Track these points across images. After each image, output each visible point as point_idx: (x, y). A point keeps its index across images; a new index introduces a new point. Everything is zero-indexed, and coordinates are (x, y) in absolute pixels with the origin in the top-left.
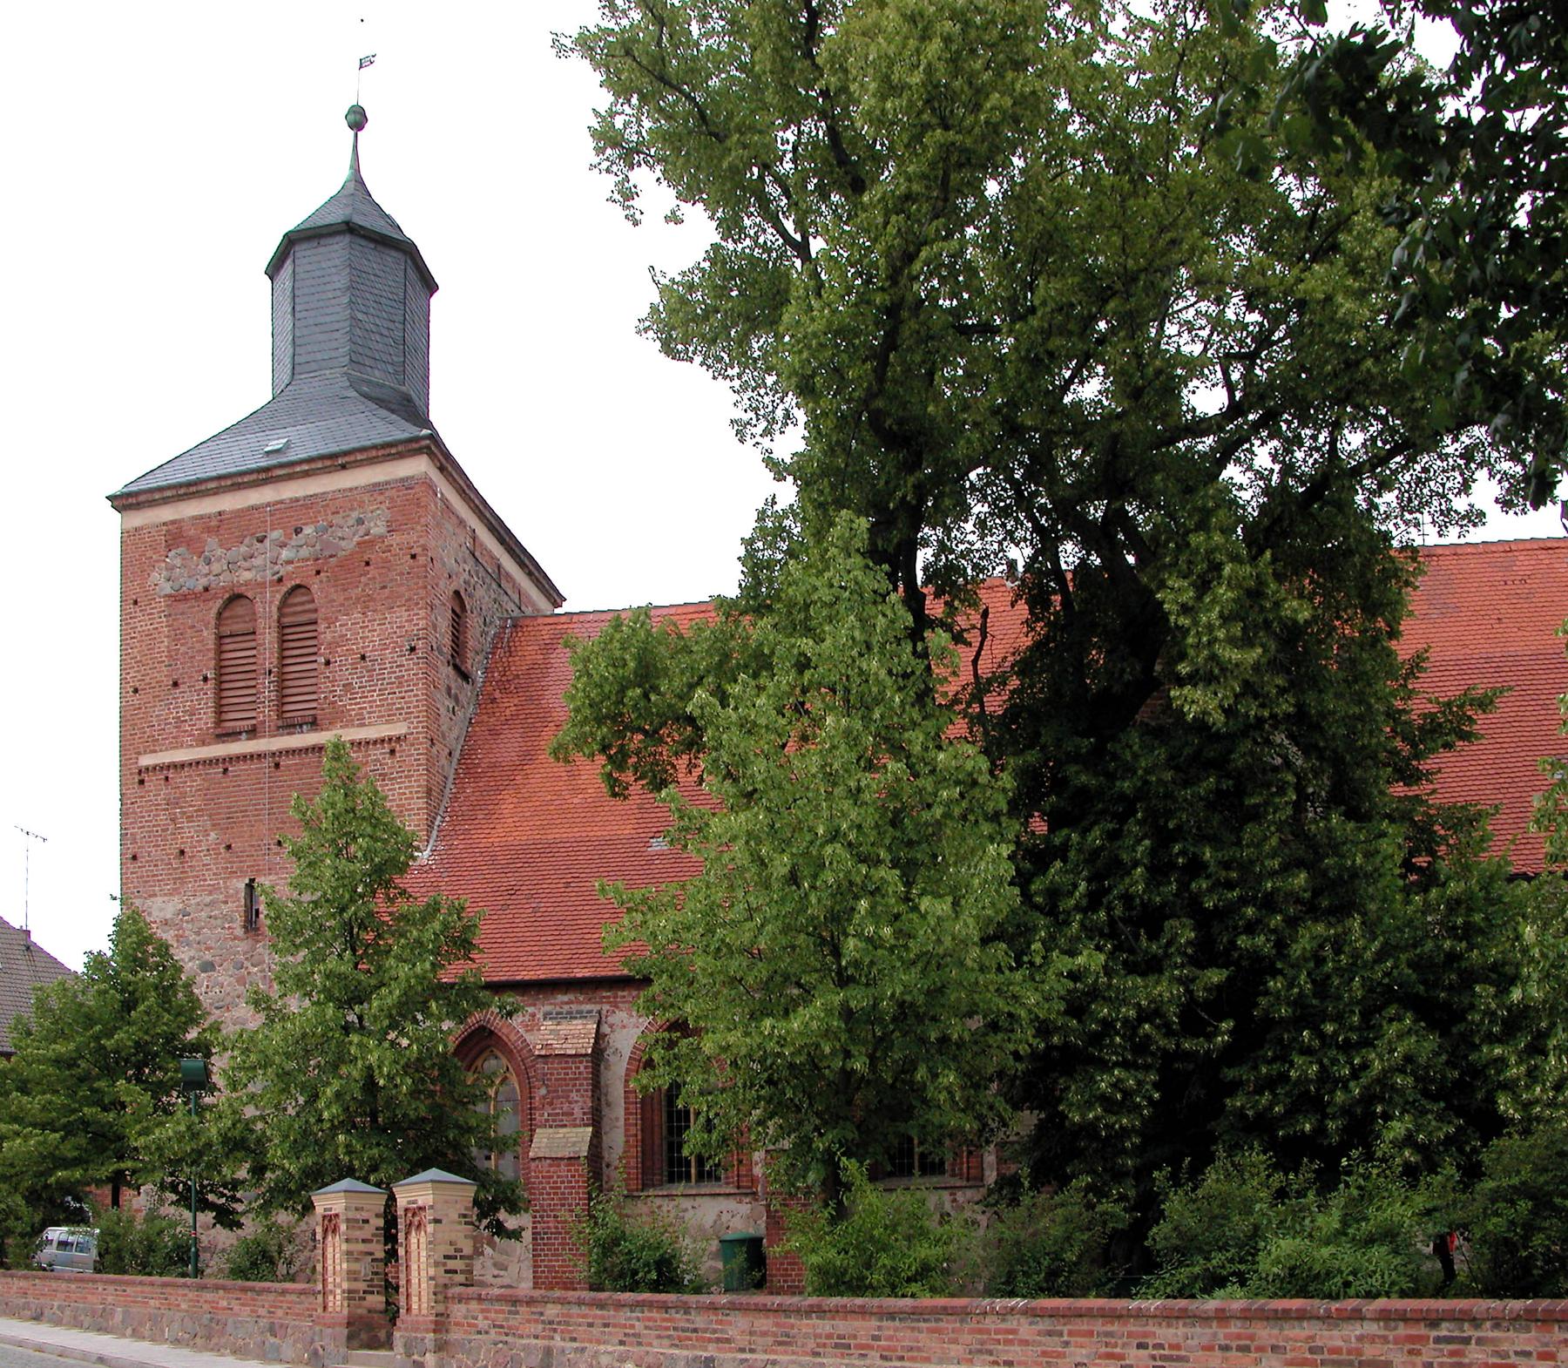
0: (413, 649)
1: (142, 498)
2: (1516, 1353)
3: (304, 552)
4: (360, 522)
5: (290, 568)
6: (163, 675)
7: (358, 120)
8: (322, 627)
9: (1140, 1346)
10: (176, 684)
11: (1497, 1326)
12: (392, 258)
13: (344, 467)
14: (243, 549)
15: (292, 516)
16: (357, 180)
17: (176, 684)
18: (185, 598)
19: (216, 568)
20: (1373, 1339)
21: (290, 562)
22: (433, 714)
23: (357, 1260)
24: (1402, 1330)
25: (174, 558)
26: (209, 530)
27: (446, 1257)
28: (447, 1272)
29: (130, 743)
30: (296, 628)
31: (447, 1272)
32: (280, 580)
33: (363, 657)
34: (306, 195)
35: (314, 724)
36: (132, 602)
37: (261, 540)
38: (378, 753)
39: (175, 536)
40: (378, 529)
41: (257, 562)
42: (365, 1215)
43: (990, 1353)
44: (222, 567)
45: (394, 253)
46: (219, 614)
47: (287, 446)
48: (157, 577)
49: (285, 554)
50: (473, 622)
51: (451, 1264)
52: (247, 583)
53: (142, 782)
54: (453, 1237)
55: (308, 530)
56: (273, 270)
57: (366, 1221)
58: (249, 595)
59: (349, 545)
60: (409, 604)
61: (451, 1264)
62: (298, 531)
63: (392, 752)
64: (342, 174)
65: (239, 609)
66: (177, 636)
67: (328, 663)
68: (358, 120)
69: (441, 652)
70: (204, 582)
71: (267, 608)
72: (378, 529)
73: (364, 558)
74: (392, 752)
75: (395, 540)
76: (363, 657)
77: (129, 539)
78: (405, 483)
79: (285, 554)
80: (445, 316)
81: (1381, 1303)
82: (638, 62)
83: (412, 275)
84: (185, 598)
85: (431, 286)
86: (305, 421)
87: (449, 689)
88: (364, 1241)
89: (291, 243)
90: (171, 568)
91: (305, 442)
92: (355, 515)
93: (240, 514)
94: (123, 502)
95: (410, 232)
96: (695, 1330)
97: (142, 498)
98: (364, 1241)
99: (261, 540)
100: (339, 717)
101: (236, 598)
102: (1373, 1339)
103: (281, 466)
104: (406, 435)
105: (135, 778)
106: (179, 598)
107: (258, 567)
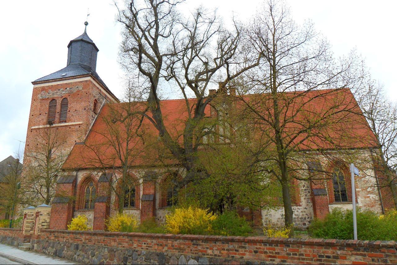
0: (85, 109)
1: (38, 83)
2: (206, 248)
3: (67, 92)
4: (78, 87)
5: (64, 95)
6: (38, 113)
7: (86, 24)
8: (69, 105)
9: (145, 244)
10: (40, 114)
11: (202, 242)
12: (90, 45)
13: (75, 78)
14: (56, 91)
15: (65, 86)
16: (85, 33)
17: (40, 114)
18: (44, 99)
19: (50, 95)
20: (182, 244)
21: (64, 94)
22: (88, 120)
23: (29, 223)
24: (187, 242)
25: (42, 93)
26: (50, 88)
27: (42, 222)
28: (42, 226)
29: (29, 125)
30: (65, 103)
31: (42, 226)
32: (62, 97)
33: (76, 110)
34: (76, 34)
35: (65, 122)
36: (34, 99)
37: (59, 90)
38: (77, 127)
39: (43, 89)
40: (81, 89)
41: (58, 94)
42: (33, 214)
43: (121, 244)
44: (51, 94)
45: (90, 45)
46: (50, 102)
47: (66, 75)
48: (39, 96)
49: (63, 92)
50: (99, 105)
51: (43, 224)
52: (56, 97)
53: (31, 131)
54: (45, 218)
55: (68, 89)
56: (69, 46)
57: (33, 215)
58: (56, 99)
59: (75, 91)
60: (85, 101)
61: (43, 224)
62: (66, 89)
63: (80, 127)
64: (83, 32)
65: (54, 101)
66: (42, 106)
67: (69, 111)
68: (86, 24)
69: (91, 109)
70: (48, 97)
71: (59, 102)
72: (81, 89)
73: (78, 93)
74: (80, 127)
75: (83, 90)
76: (76, 110)
77: (35, 91)
78: (86, 81)
79: (63, 92)
80: (99, 54)
81: (185, 235)
82: (338, 114)
83: (94, 48)
84: (44, 99)
85: (97, 50)
86: (70, 71)
87: (92, 116)
88: (31, 219)
89: (71, 43)
90: (42, 94)
91: (70, 74)
92: (77, 86)
93: (55, 86)
94: (34, 83)
95: (94, 42)
96: (77, 238)
97: (38, 83)
98: (31, 219)
99: (59, 90)
100: (70, 120)
101: (53, 100)
102: (182, 244)
103: (64, 78)
104: (86, 73)
105: (30, 130)
106: (43, 99)
107: (58, 95)
